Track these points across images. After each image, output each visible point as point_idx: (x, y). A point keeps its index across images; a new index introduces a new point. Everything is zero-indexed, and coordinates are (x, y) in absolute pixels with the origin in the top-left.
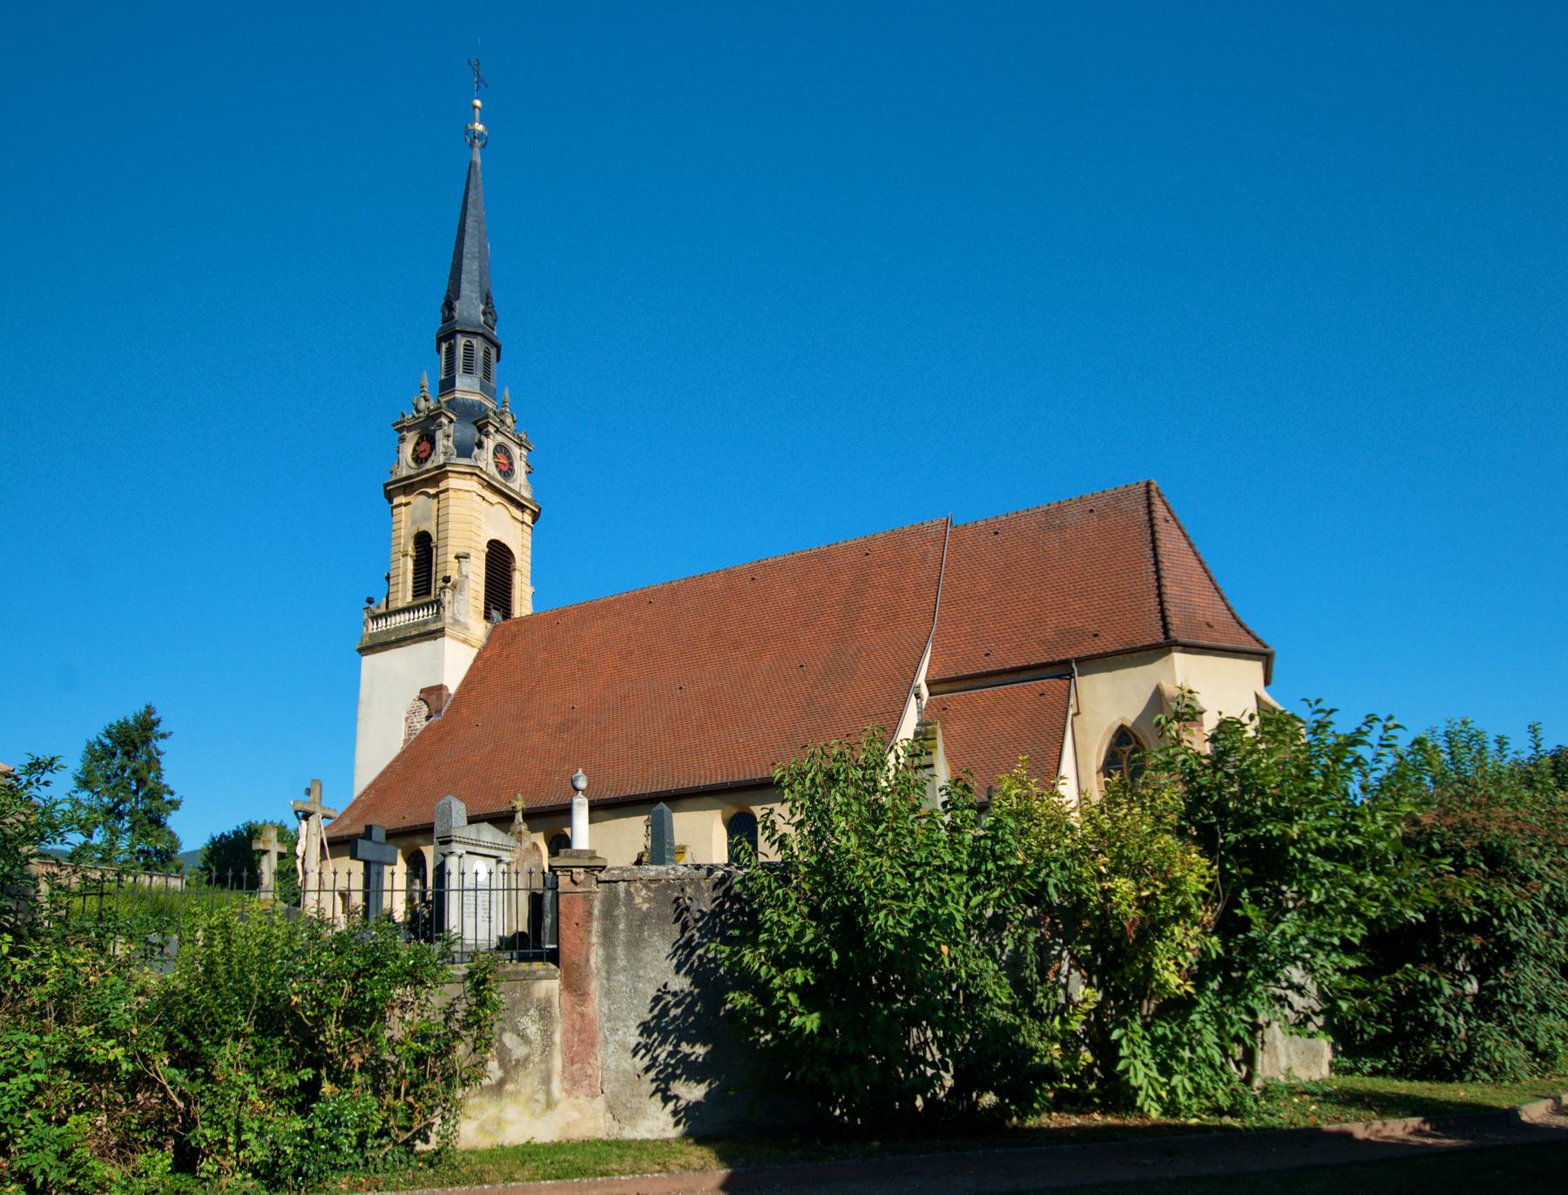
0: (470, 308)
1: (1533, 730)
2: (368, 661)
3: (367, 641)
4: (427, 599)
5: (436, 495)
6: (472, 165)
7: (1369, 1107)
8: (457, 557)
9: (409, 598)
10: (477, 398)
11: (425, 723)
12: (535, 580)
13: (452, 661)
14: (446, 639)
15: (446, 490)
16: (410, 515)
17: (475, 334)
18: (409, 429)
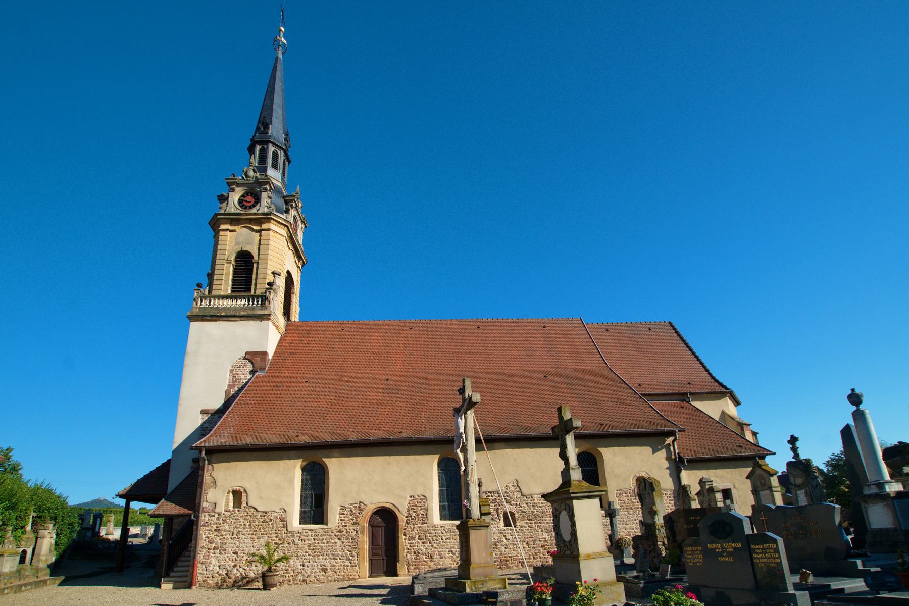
0: (276, 130)
1: (793, 440)
2: (195, 326)
3: (196, 312)
4: (246, 294)
5: (259, 231)
6: (277, 58)
7: (462, 559)
8: (273, 273)
9: (229, 292)
10: (280, 185)
11: (249, 376)
12: (301, 304)
13: (268, 337)
14: (270, 322)
15: (269, 230)
16: (232, 240)
17: (281, 148)
18: (238, 185)
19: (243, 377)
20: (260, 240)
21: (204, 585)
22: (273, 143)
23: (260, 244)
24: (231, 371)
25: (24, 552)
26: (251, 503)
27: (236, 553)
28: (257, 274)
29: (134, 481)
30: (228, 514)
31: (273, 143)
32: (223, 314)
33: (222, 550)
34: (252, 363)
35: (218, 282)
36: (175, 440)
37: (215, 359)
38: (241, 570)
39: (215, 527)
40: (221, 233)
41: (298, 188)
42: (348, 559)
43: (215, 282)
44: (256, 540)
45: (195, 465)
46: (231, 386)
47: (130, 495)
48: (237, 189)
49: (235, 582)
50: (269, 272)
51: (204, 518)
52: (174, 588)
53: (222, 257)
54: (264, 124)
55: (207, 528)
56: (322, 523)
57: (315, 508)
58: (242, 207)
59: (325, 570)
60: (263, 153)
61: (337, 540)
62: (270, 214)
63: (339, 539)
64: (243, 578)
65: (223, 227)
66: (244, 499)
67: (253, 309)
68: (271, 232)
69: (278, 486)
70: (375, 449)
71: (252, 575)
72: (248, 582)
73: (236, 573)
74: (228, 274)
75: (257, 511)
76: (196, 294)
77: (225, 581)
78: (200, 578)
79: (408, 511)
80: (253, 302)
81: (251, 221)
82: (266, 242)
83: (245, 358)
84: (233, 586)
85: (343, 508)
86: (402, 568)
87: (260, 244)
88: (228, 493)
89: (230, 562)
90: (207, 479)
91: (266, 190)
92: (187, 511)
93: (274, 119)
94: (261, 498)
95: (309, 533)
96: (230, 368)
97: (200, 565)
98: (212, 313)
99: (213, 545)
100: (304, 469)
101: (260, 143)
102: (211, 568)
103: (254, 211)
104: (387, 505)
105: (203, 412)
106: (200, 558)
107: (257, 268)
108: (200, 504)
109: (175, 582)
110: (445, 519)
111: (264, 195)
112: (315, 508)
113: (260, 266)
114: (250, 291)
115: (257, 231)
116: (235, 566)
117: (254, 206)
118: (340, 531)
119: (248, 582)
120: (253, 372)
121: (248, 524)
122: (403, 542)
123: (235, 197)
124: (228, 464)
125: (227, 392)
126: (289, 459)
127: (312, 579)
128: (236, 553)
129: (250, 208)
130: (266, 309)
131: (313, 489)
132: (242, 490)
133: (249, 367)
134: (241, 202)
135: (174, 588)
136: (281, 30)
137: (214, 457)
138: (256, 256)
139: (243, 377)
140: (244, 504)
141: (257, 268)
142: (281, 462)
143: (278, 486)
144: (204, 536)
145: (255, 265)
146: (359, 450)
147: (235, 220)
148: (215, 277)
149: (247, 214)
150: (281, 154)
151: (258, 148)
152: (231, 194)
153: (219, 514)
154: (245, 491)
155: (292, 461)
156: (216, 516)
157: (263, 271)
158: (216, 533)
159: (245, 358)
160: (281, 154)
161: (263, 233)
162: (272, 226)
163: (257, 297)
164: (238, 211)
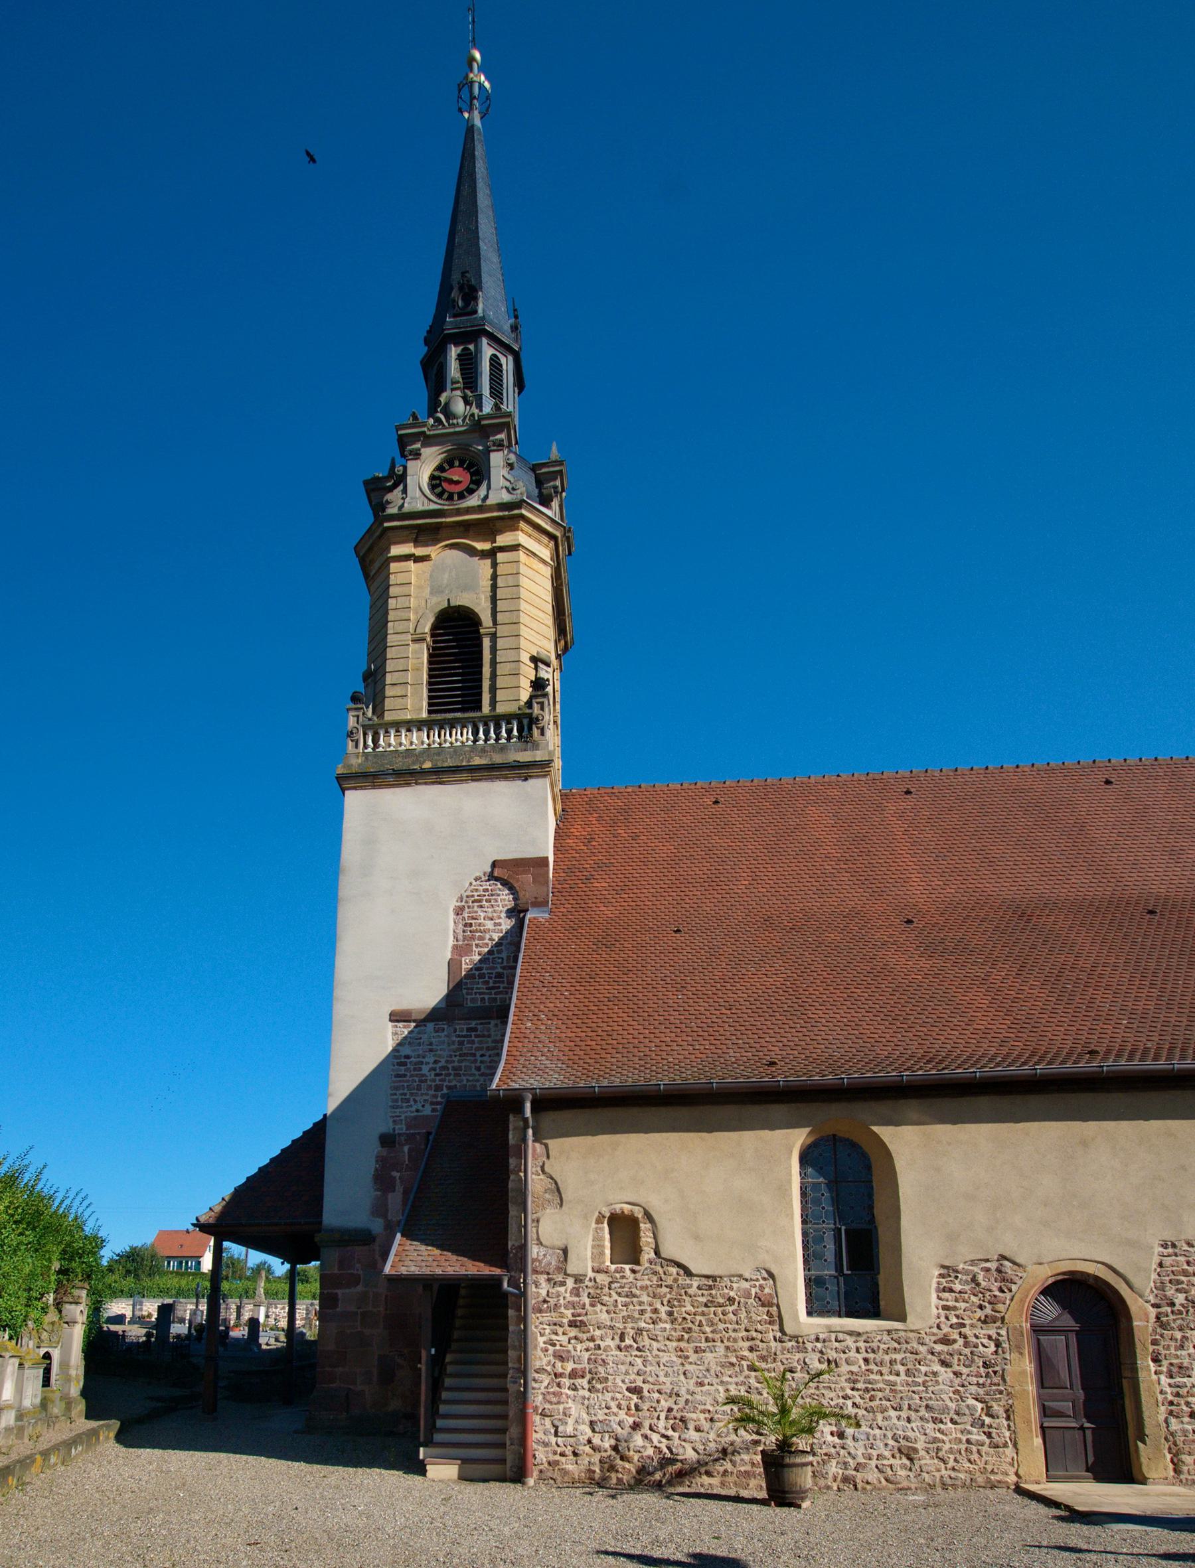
0: (491, 305)
2: (355, 800)
3: (356, 763)
5: (491, 554)
6: (470, 129)
15: (515, 547)
16: (424, 582)
17: (508, 348)
18: (428, 440)
19: (489, 925)
20: (494, 577)
21: (554, 1477)
22: (492, 338)
23: (494, 587)
24: (459, 911)
25: (47, 1356)
26: (668, 1251)
27: (636, 1391)
28: (494, 663)
29: (227, 1191)
30: (602, 1279)
31: (492, 338)
32: (428, 765)
33: (596, 1381)
34: (511, 889)
35: (397, 691)
36: (331, 1088)
37: (416, 879)
38: (655, 1437)
39: (568, 1313)
40: (394, 566)
41: (554, 448)
42: (978, 1423)
43: (389, 691)
44: (693, 1357)
45: (384, 1152)
46: (460, 950)
47: (225, 1226)
48: (427, 452)
49: (642, 1471)
50: (525, 658)
51: (538, 1289)
52: (463, 1477)
53: (401, 627)
54: (459, 287)
55: (547, 1317)
56: (875, 1314)
57: (856, 1264)
58: (439, 496)
59: (909, 1454)
60: (469, 364)
61: (937, 1367)
62: (518, 504)
63: (944, 1363)
64: (665, 1462)
65: (395, 550)
66: (646, 1238)
67: (503, 749)
68: (522, 555)
69: (737, 1201)
70: (1035, 1101)
71: (690, 1455)
72: (681, 1475)
73: (643, 1447)
74: (418, 669)
75: (688, 1273)
76: (352, 722)
77: (612, 1468)
78: (541, 1455)
79: (1161, 1287)
80: (486, 733)
81: (467, 528)
82: (511, 581)
83: (491, 877)
84: (638, 1482)
85: (949, 1271)
86: (1153, 1458)
87: (494, 587)
88: (599, 1221)
89: (622, 1415)
90: (536, 1183)
91: (500, 445)
92: (486, 1270)
93: (485, 278)
94: (697, 1238)
95: (850, 1341)
96: (454, 904)
97: (537, 1419)
98: (399, 764)
99: (570, 1366)
100: (805, 1158)
101: (457, 339)
102: (569, 1429)
103: (473, 501)
104: (1090, 1268)
105: (397, 1017)
106: (536, 1399)
107: (494, 650)
108: (523, 1248)
109: (465, 1461)
110: (821, 1314)
111: (497, 459)
112: (856, 1264)
113: (501, 643)
114: (479, 708)
115: (484, 554)
116: (636, 1426)
117: (471, 492)
118: (945, 1341)
119: (681, 1475)
120: (517, 913)
121: (663, 1310)
122: (1153, 1382)
123: (421, 472)
124: (589, 1139)
125: (453, 965)
126: (772, 1127)
127: (873, 1476)
128: (636, 1391)
129: (461, 496)
130: (536, 746)
131: (840, 1215)
132: (639, 1214)
133: (505, 899)
134: (436, 482)
135: (463, 1477)
136: (473, 59)
137: (549, 1118)
138: (486, 619)
139: (489, 925)
140: (648, 1254)
141: (494, 650)
142: (748, 1135)
143: (737, 1201)
144: (543, 1339)
145: (486, 642)
146: (983, 1102)
147: (427, 531)
148: (389, 679)
149: (459, 512)
150: (507, 363)
151: (454, 352)
152: (410, 464)
153: (578, 1279)
154: (648, 1216)
155: (779, 1134)
156: (570, 1283)
157: (511, 655)
158: (573, 1332)
159: (491, 877)
160: (507, 363)
161: (501, 557)
162: (522, 537)
163: (508, 718)
164: (433, 507)
